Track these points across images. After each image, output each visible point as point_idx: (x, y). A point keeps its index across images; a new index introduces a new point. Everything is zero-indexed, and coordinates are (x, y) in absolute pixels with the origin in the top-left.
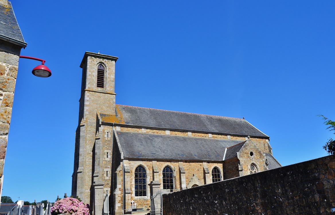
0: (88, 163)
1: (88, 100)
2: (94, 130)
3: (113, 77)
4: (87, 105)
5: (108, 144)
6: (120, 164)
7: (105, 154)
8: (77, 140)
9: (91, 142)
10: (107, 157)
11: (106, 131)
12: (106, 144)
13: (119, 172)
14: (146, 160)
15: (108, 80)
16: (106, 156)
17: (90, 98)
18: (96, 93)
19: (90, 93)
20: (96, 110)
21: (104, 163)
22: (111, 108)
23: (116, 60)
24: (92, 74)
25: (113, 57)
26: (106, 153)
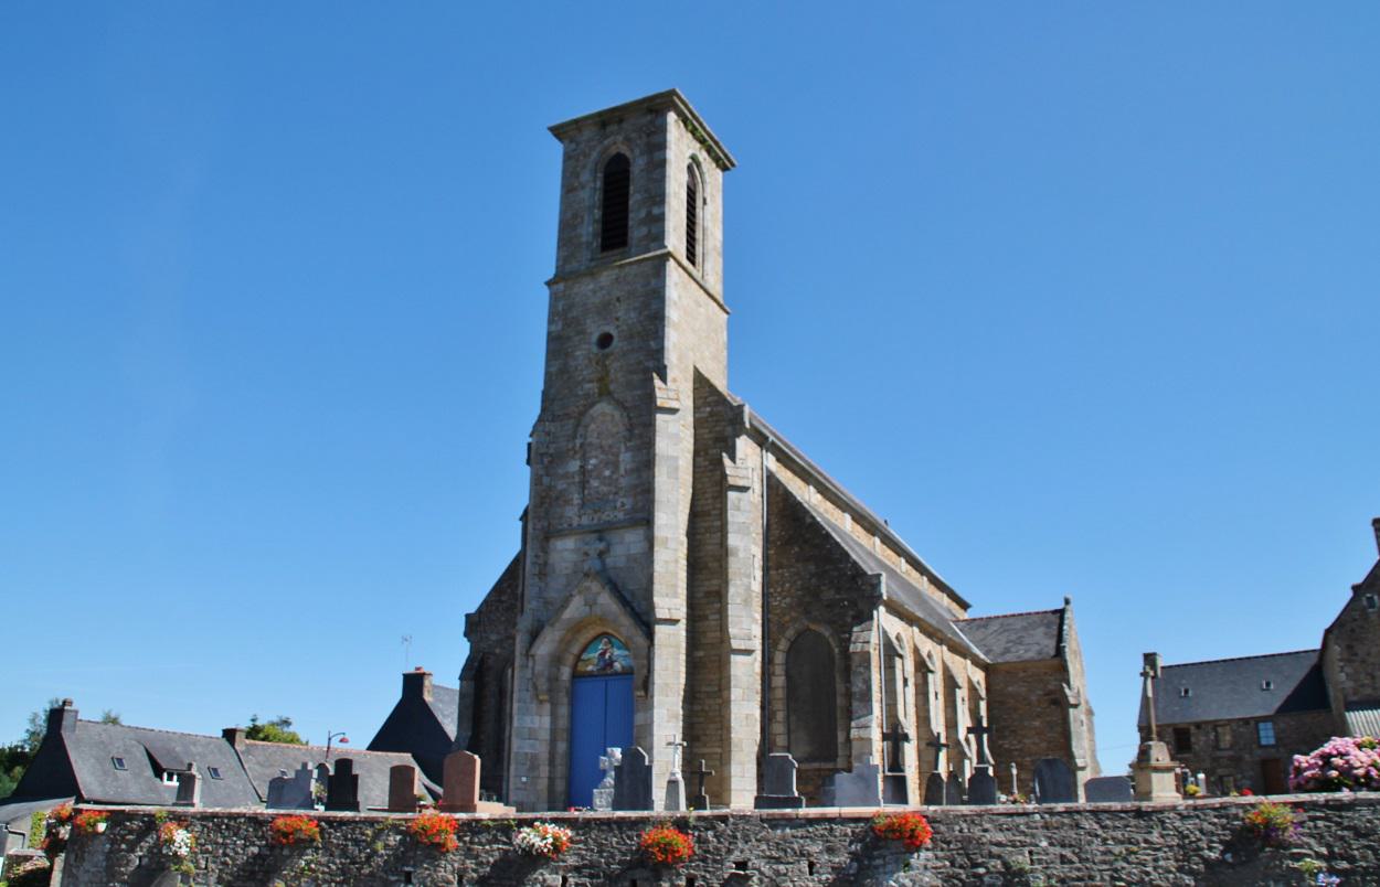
25: (726, 155)
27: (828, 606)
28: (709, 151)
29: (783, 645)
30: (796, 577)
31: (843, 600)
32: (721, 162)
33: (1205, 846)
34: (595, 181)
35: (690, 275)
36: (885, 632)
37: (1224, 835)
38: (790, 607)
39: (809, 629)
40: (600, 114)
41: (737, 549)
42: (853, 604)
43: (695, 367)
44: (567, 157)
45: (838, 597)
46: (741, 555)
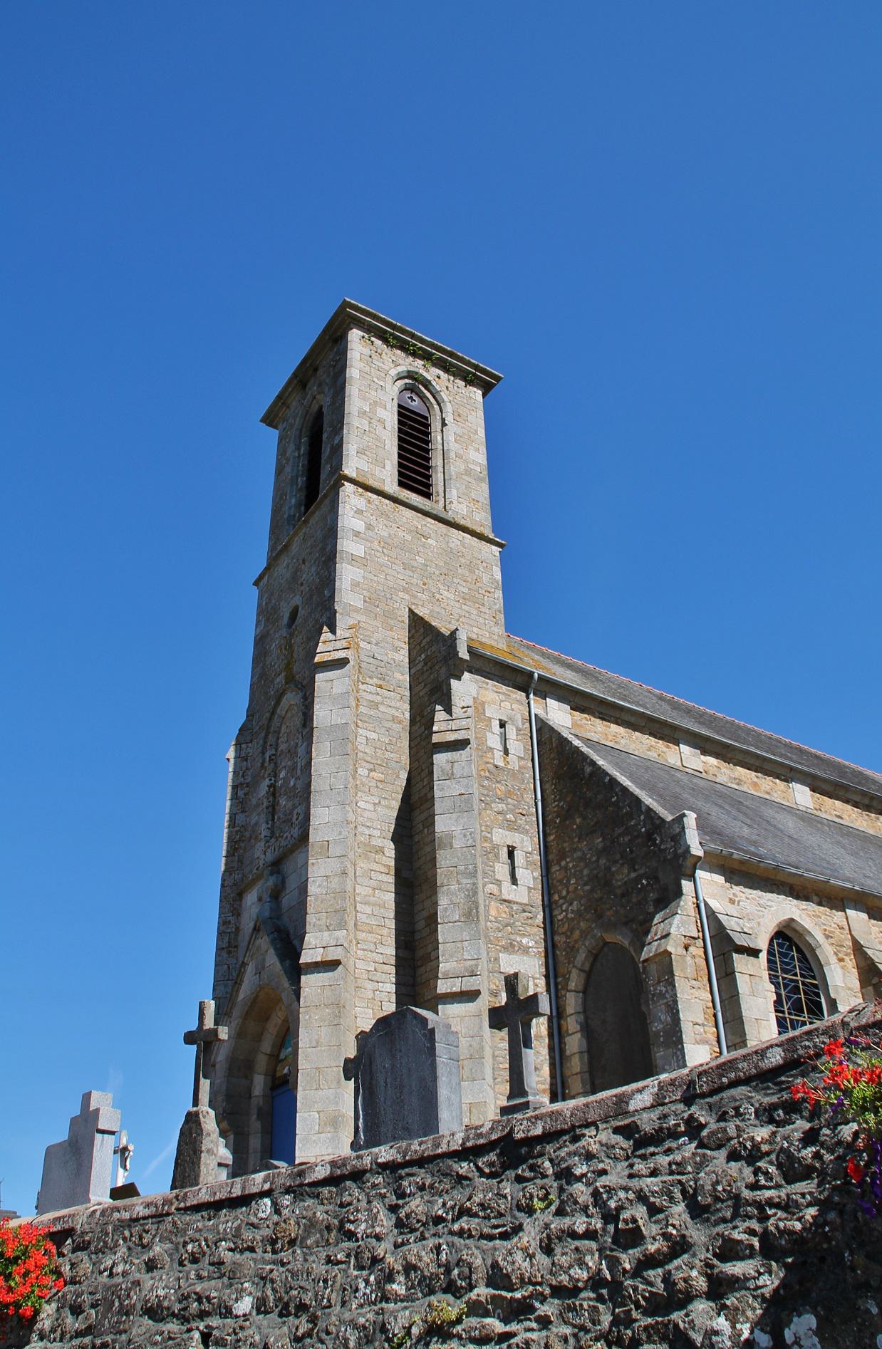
0: (368, 910)
1: (357, 534)
2: (397, 709)
3: (478, 457)
4: (353, 559)
5: (509, 794)
6: (679, 893)
7: (497, 856)
8: (241, 793)
9: (381, 777)
10: (514, 881)
11: (493, 713)
12: (500, 789)
13: (681, 951)
14: (815, 898)
15: (455, 468)
16: (502, 870)
17: (369, 527)
18: (401, 507)
19: (369, 502)
20: (407, 597)
21: (493, 912)
22: (482, 609)
23: (487, 388)
24: (373, 411)
25: (476, 367)
26: (505, 850)
27: (623, 895)
28: (426, 357)
29: (575, 980)
30: (582, 864)
31: (638, 879)
32: (434, 358)
33: (701, 1283)
34: (299, 449)
35: (426, 514)
36: (712, 914)
37: (788, 1206)
38: (579, 914)
39: (606, 944)
40: (295, 375)
41: (451, 836)
42: (654, 878)
43: (410, 609)
44: (281, 439)
45: (633, 875)
46: (457, 844)
